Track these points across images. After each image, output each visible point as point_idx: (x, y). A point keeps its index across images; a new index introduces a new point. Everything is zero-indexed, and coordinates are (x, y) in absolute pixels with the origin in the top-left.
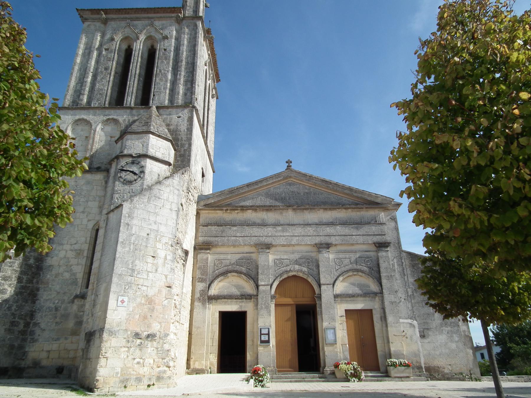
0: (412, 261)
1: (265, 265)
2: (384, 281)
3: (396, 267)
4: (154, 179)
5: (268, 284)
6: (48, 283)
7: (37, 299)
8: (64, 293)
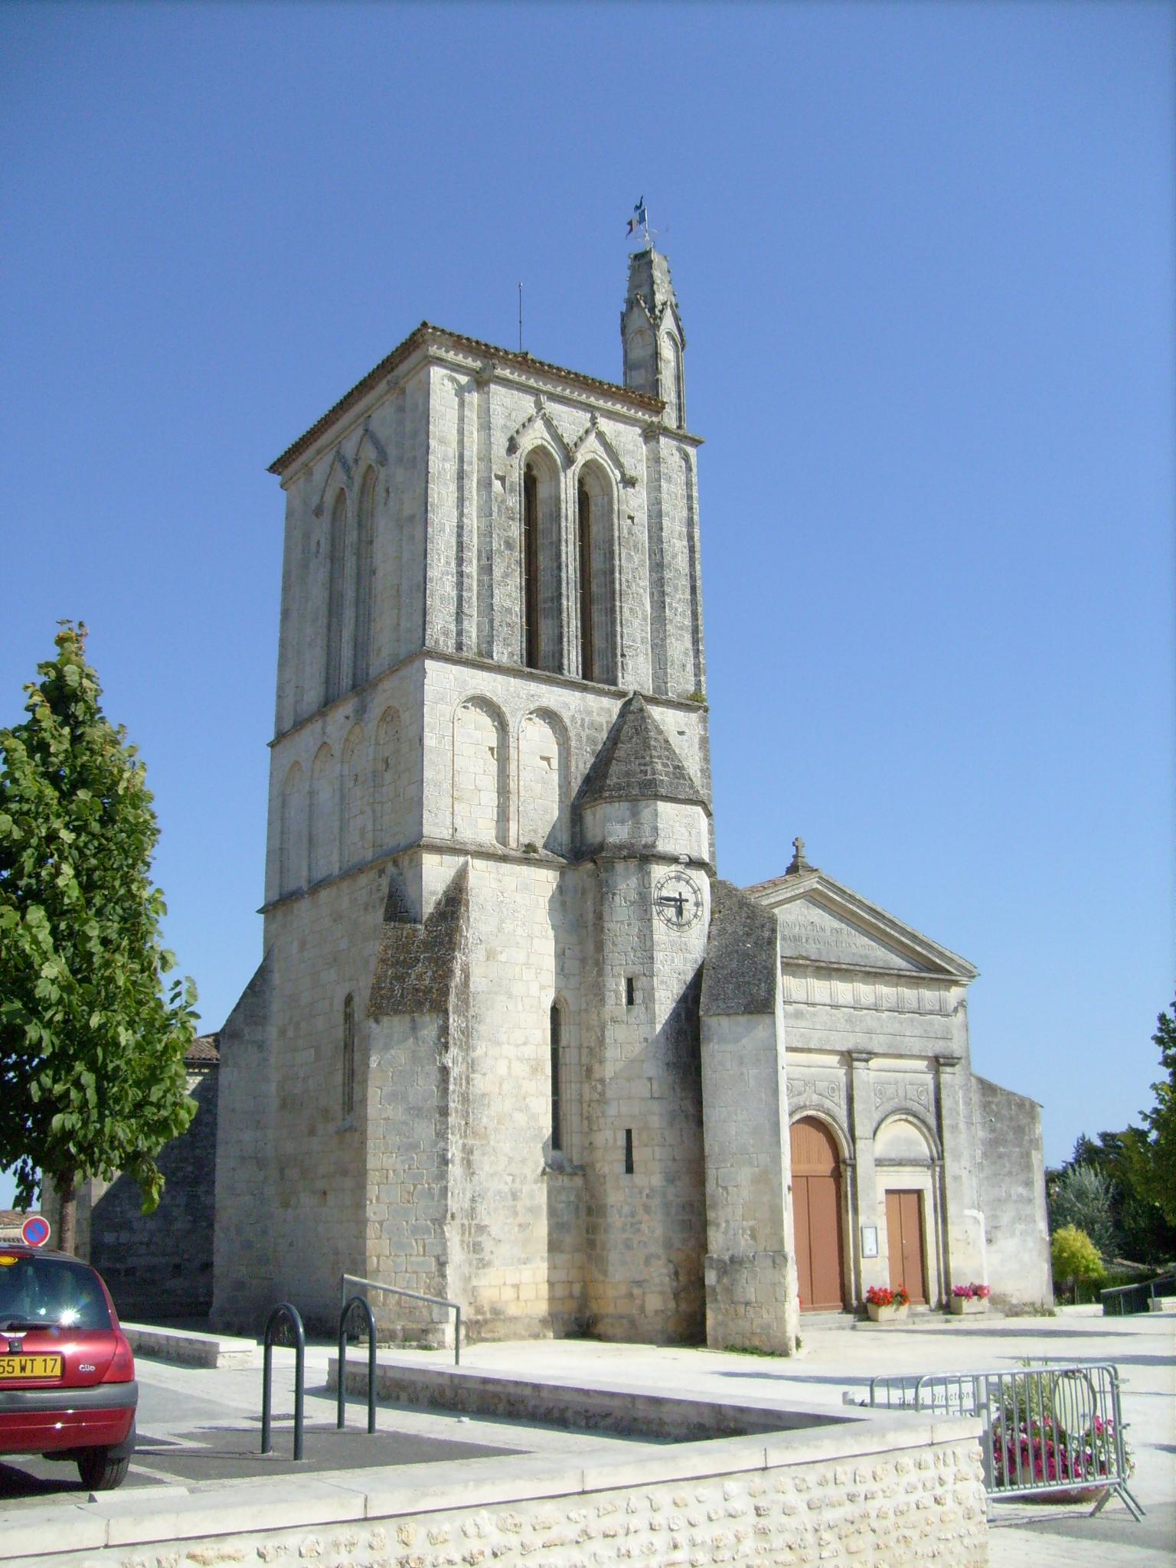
0: (984, 1095)
6: (486, 1136)
8: (524, 1161)
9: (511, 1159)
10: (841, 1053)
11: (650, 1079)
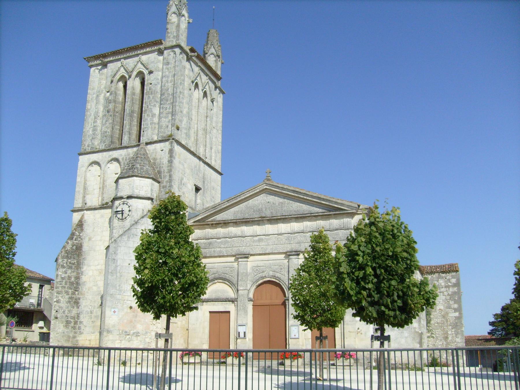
1: (244, 272)
4: (139, 214)
5: (248, 289)
8: (95, 302)
10: (285, 253)
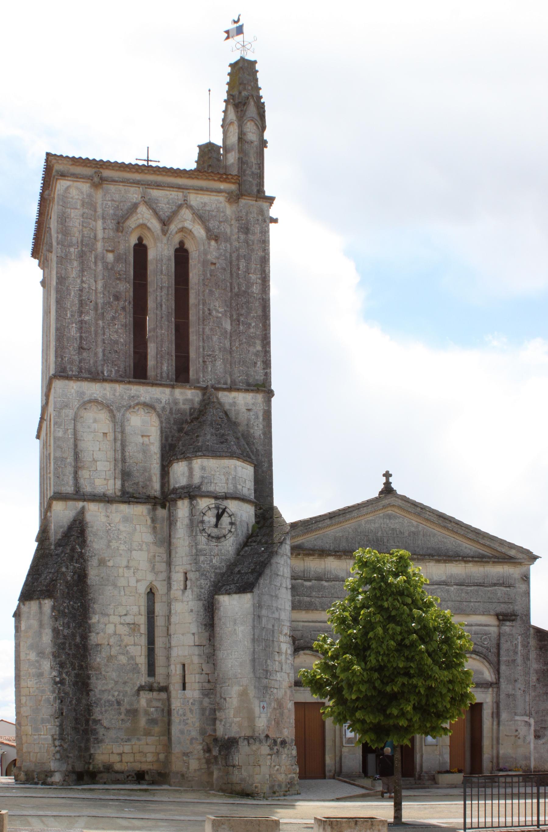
0: (540, 640)
2: (503, 668)
3: (520, 647)
6: (99, 669)
7: (91, 690)
9: (116, 683)
11: (194, 634)
